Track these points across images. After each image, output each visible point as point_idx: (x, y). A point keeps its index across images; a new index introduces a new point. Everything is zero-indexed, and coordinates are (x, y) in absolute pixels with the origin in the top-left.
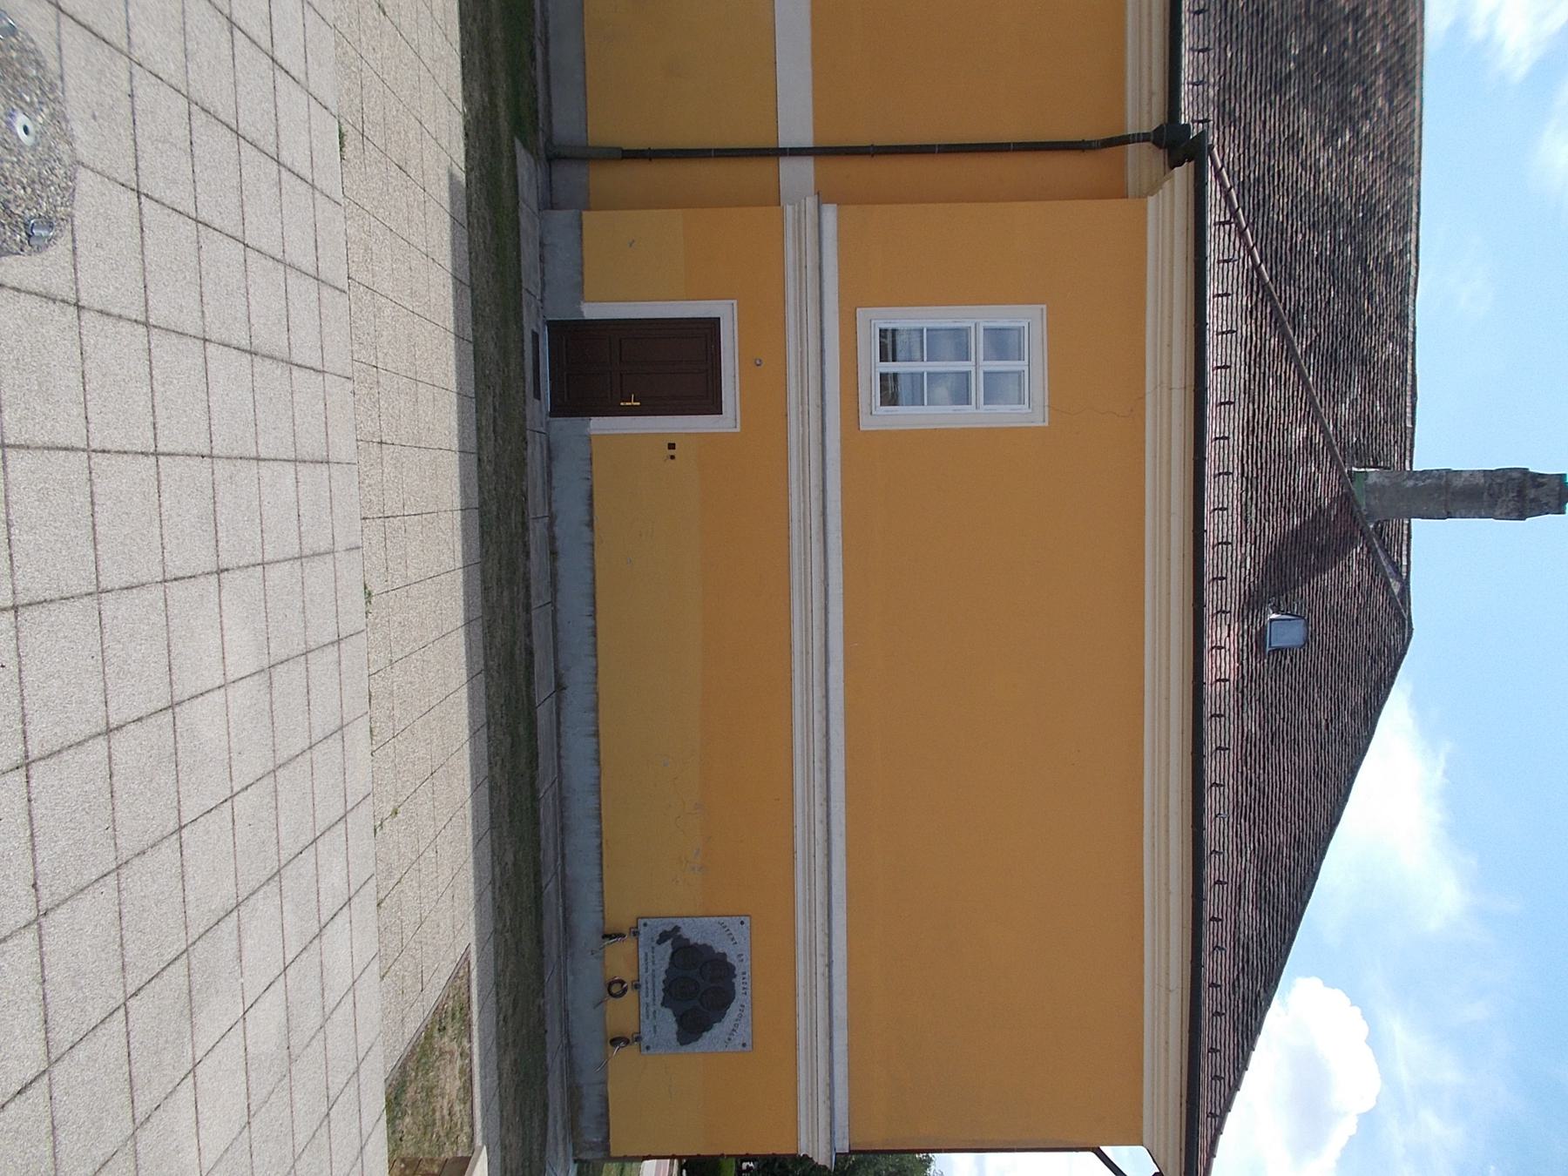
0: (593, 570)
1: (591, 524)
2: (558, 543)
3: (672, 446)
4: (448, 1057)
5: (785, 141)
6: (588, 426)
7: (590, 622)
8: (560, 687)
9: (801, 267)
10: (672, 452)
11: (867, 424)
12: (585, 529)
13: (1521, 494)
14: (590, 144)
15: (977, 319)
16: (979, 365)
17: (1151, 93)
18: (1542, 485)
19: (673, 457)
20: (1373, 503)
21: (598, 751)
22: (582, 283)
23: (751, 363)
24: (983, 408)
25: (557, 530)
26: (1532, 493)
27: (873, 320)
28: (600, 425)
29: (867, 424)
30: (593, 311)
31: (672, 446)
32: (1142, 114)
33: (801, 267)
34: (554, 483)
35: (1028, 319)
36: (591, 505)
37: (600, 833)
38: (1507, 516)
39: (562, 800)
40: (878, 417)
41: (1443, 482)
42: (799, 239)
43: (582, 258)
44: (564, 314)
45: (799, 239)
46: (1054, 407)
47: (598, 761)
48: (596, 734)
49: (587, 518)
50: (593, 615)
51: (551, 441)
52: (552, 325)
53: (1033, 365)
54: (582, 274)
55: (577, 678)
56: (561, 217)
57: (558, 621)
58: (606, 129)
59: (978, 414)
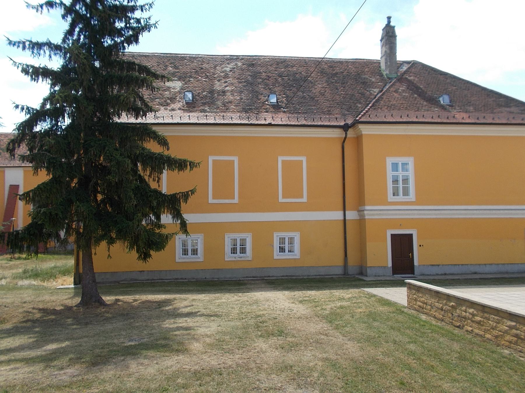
0: (449, 265)
1: (438, 265)
2: (443, 273)
3: (420, 246)
4: (352, 311)
5: (342, 218)
6: (416, 266)
7: (460, 266)
8: (475, 273)
9: (380, 215)
10: (421, 246)
11: (414, 200)
12: (440, 266)
13: (391, 36)
14: (343, 265)
15: (390, 174)
16: (400, 174)
17: (333, 131)
18: (388, 31)
19: (423, 246)
20: (393, 72)
21: (489, 264)
22: (384, 267)
23: (400, 227)
24: (410, 172)
25: (440, 273)
26: (391, 34)
27: (391, 198)
28: (416, 263)
29: (414, 200)
30: (390, 264)
31: (420, 246)
32: (338, 133)
33: (380, 215)
34: (429, 274)
35: (390, 161)
36: (434, 265)
37: (508, 264)
38: (395, 39)
39: (501, 273)
40: (412, 196)
41: (388, 55)
42: (373, 215)
43: (378, 267)
44: (390, 272)
45: (373, 215)
46: (409, 155)
47: (491, 264)
48: (485, 264)
49: (437, 266)
50: (459, 265)
51: (420, 274)
52: (393, 274)
53: (400, 160)
54: (382, 267)
55: (473, 269)
56: (369, 271)
57: (460, 273)
58: (339, 262)
59: (411, 174)
